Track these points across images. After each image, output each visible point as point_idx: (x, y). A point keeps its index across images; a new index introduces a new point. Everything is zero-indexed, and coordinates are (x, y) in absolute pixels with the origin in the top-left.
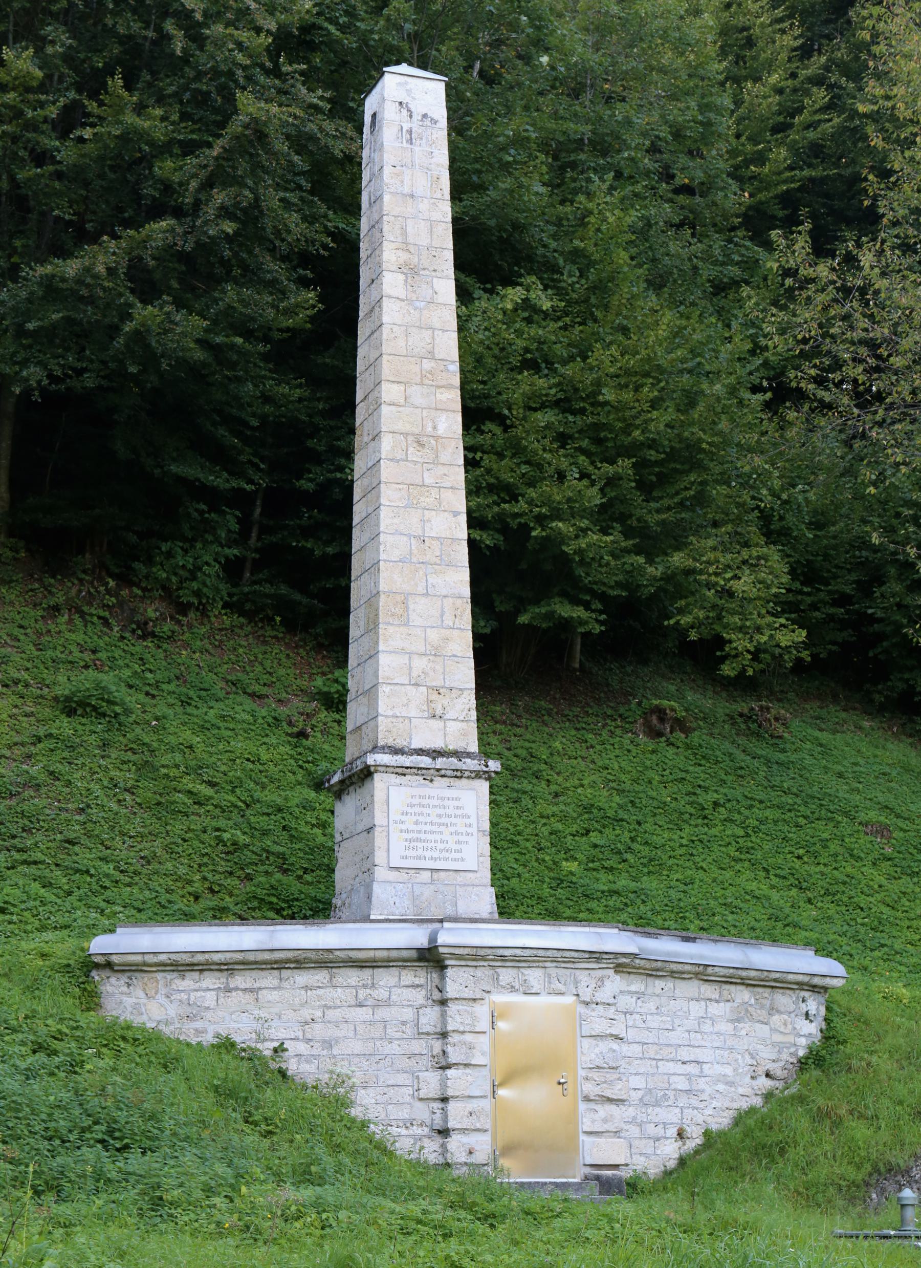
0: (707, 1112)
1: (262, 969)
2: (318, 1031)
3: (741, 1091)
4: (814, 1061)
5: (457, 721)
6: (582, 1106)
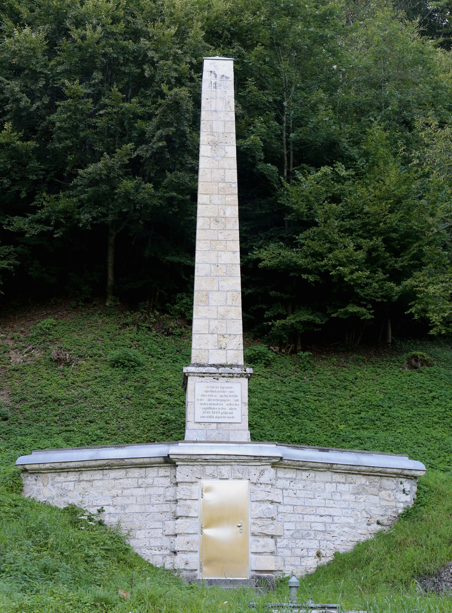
0: (336, 543)
1: (95, 470)
2: (119, 501)
3: (360, 531)
4: (407, 515)
5: (233, 349)
6: (251, 539)
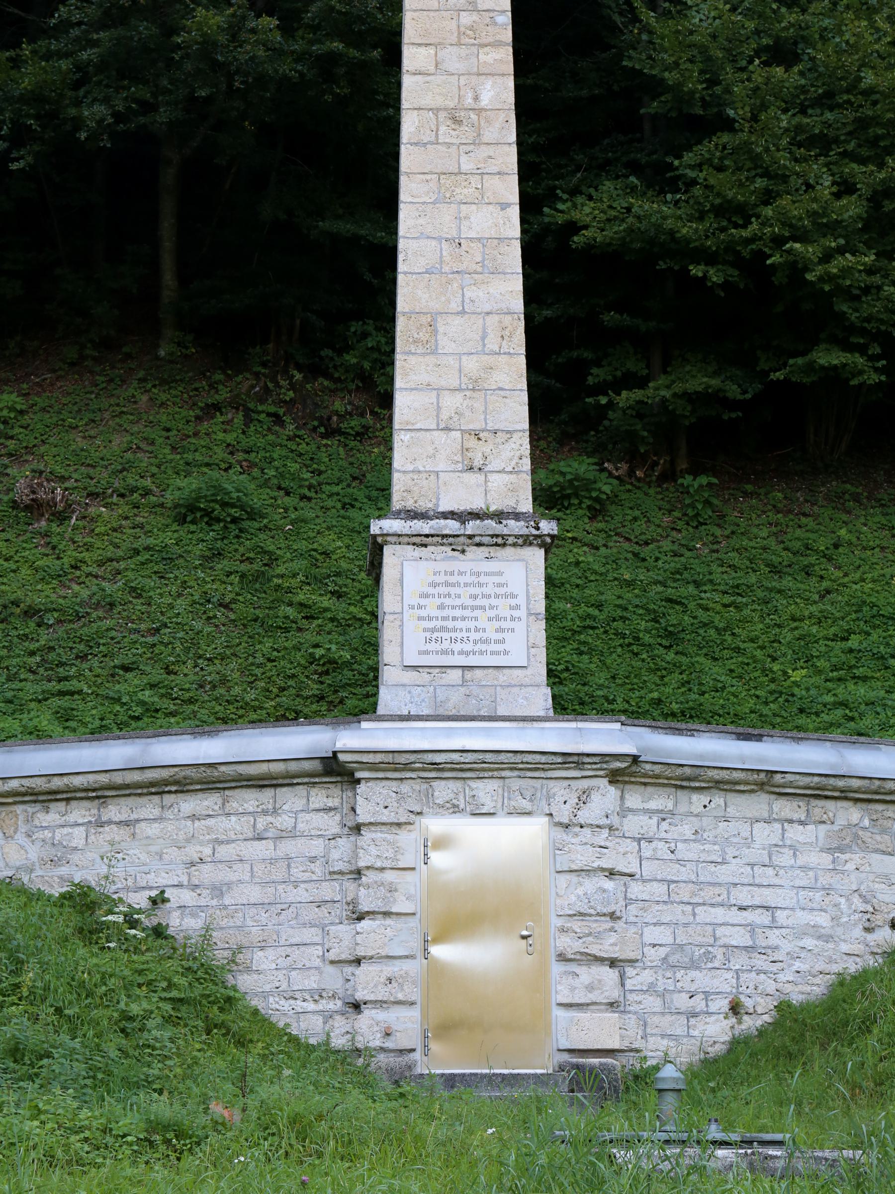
0: (781, 977)
1: (140, 795)
2: (207, 874)
3: (845, 947)
5: (507, 476)
6: (557, 968)
